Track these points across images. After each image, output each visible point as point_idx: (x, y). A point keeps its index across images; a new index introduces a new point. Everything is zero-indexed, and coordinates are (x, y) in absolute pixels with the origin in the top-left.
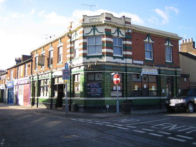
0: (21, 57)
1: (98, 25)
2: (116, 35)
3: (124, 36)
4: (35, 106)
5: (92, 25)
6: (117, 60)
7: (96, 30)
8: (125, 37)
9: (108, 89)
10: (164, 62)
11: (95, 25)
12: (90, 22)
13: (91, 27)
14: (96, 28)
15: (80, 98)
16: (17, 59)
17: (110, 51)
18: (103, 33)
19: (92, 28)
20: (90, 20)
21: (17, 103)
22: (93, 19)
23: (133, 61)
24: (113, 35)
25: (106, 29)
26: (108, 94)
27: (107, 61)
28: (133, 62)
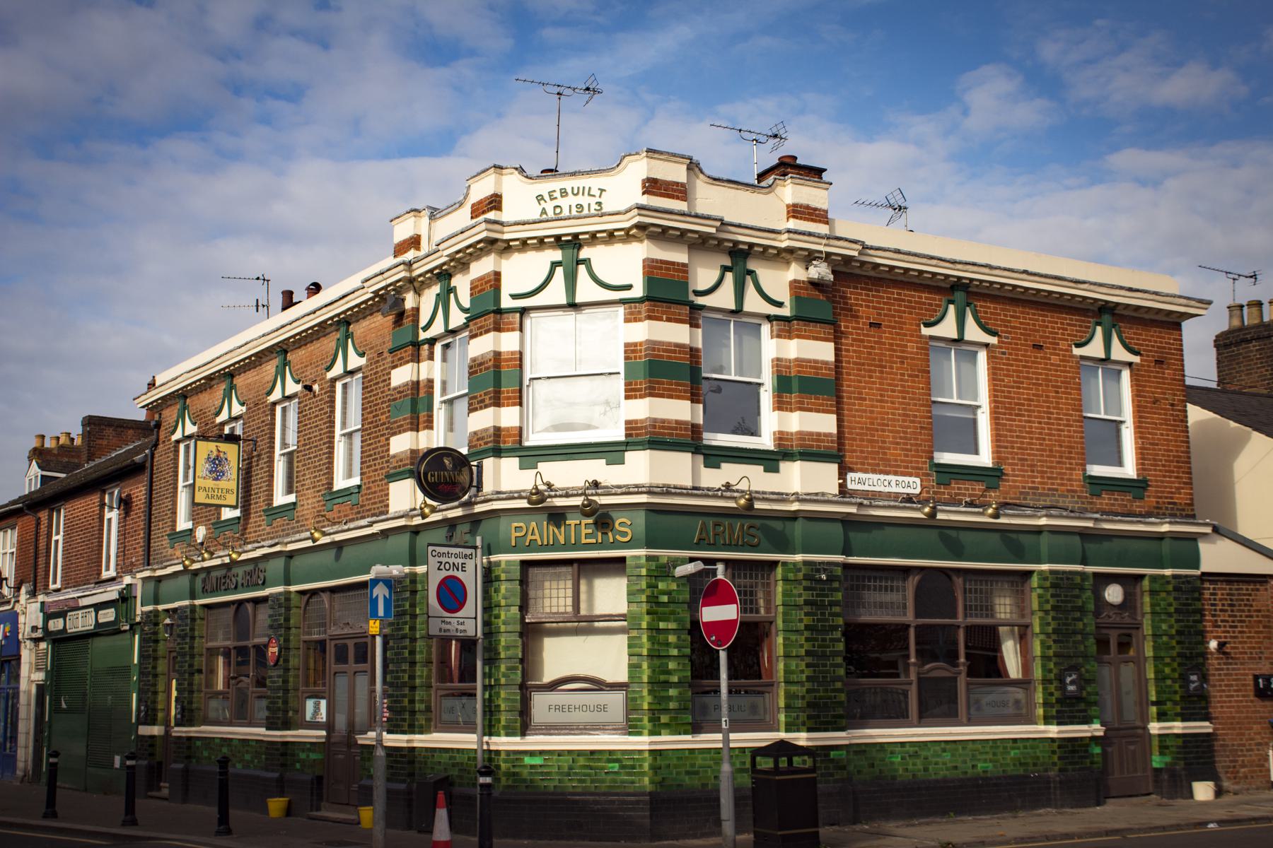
0: (77, 431)
1: (593, 235)
2: (724, 298)
3: (779, 304)
4: (230, 696)
5: (558, 238)
6: (730, 473)
7: (582, 268)
8: (786, 311)
9: (669, 672)
10: (1077, 474)
11: (576, 236)
12: (544, 212)
13: (551, 246)
14: (585, 253)
15: (262, 730)
16: (49, 444)
17: (679, 410)
18: (629, 287)
19: (557, 255)
20: (540, 198)
21: (758, 611)
22: (564, 193)
23: (842, 474)
24: (701, 301)
25: (652, 268)
26: (666, 710)
27: (661, 481)
28: (842, 487)
